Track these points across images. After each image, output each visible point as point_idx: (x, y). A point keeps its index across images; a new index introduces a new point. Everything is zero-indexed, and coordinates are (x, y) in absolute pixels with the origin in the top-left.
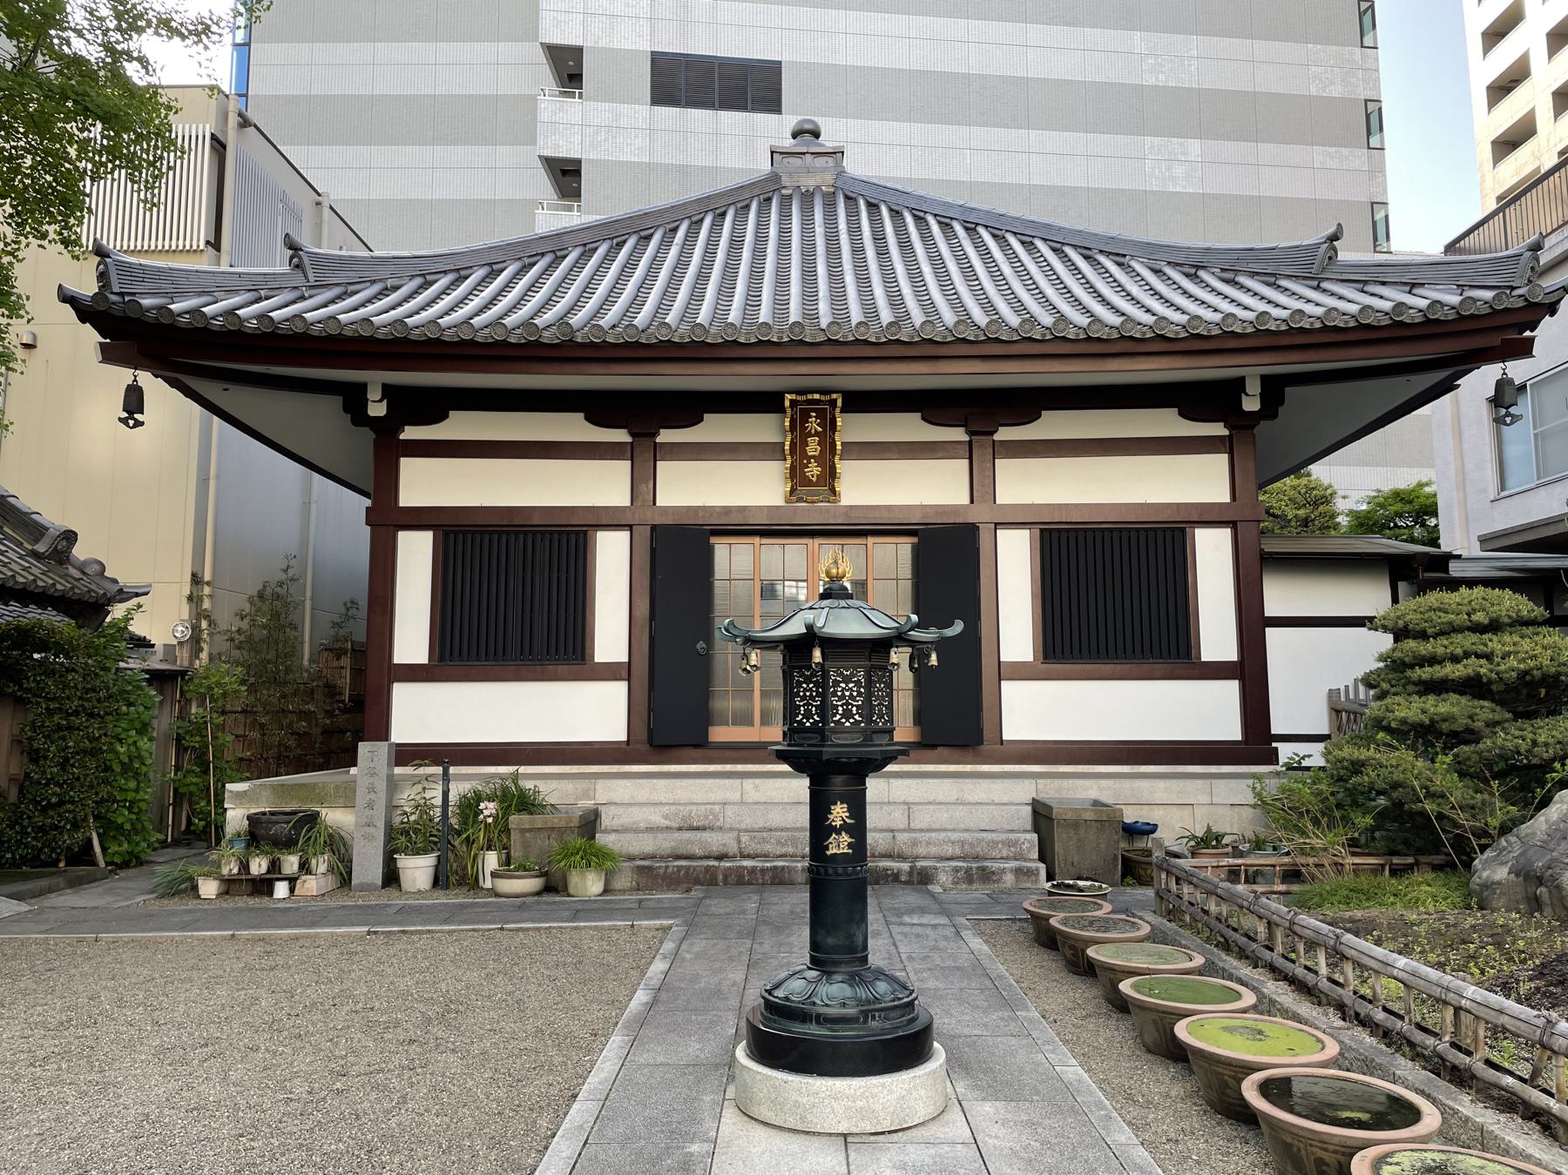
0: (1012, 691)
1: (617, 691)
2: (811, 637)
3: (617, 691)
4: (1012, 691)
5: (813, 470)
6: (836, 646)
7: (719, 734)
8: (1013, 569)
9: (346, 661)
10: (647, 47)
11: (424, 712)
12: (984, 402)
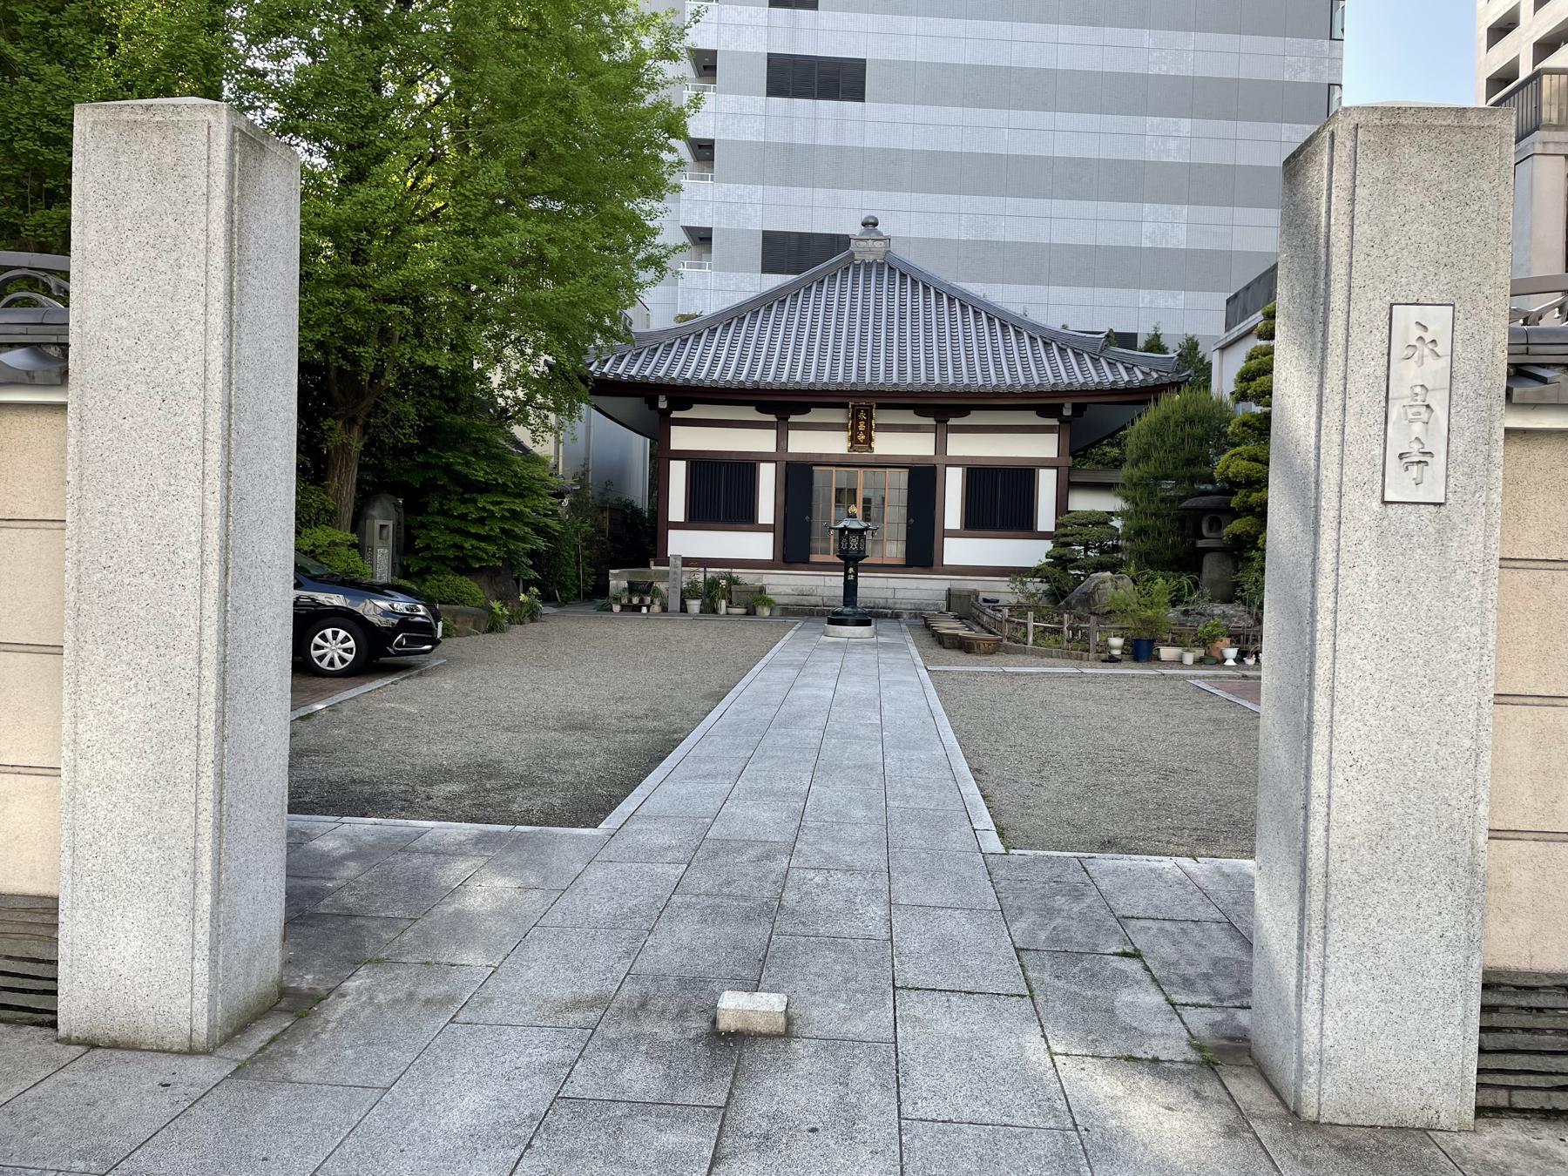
0: (949, 543)
1: (768, 538)
2: (845, 528)
3: (768, 538)
4: (949, 543)
5: (862, 437)
6: (852, 531)
7: (814, 558)
8: (954, 483)
9: (606, 514)
10: (764, 50)
11: (682, 543)
12: (943, 408)
